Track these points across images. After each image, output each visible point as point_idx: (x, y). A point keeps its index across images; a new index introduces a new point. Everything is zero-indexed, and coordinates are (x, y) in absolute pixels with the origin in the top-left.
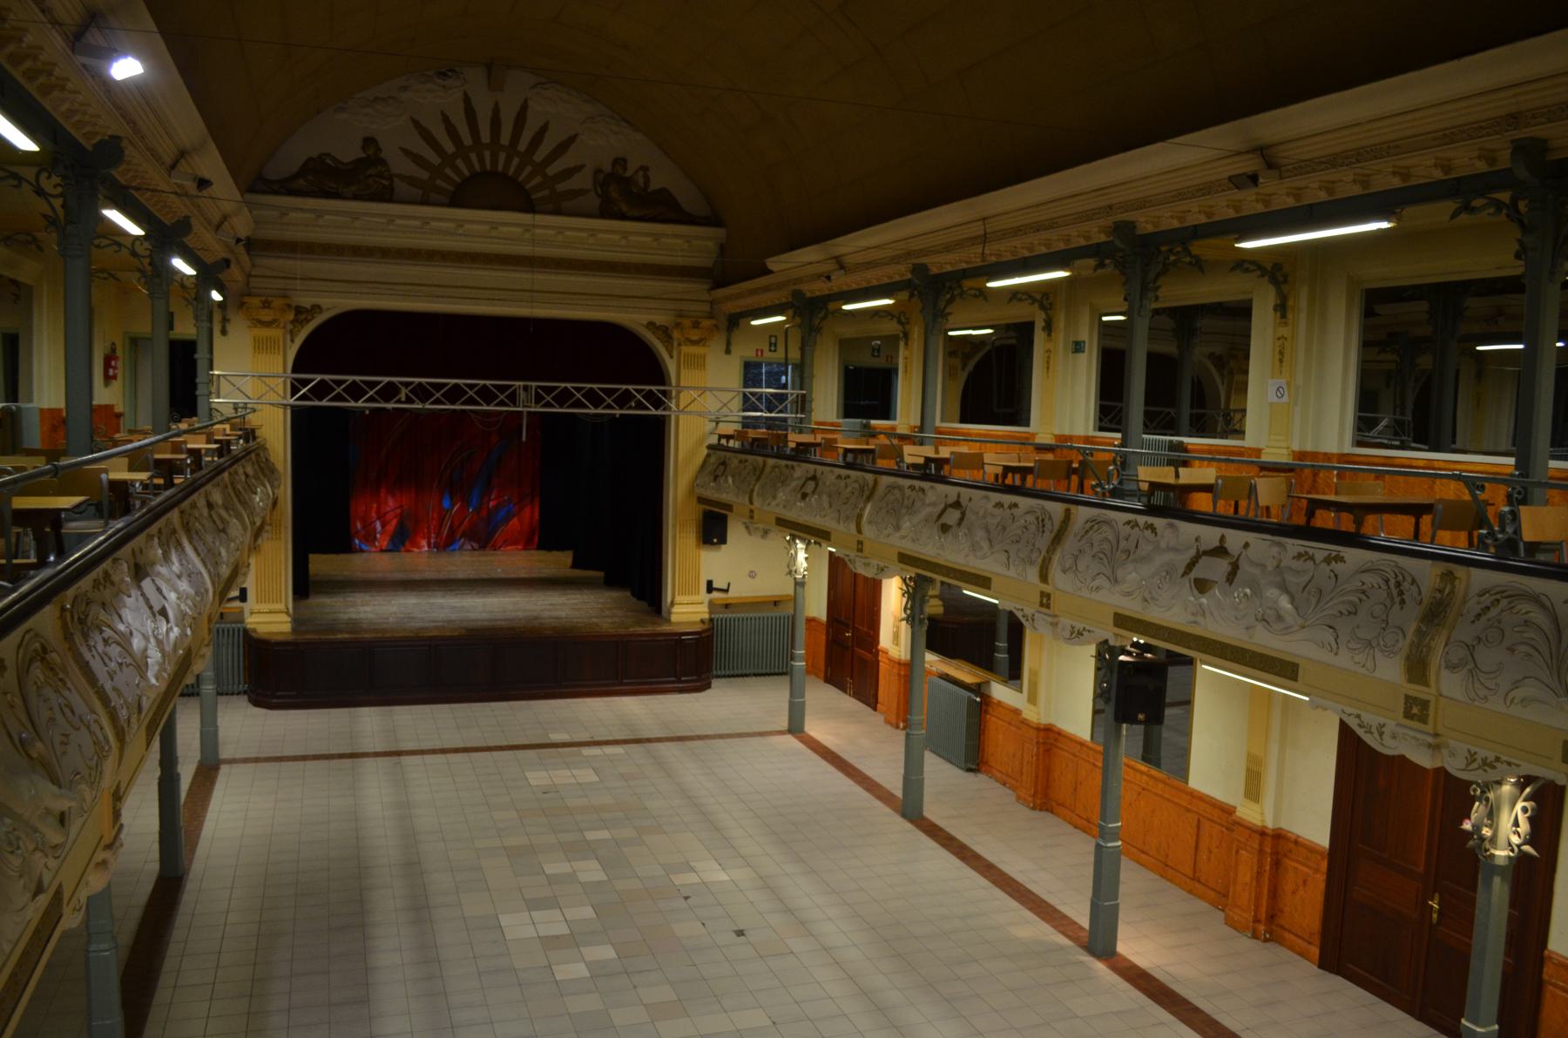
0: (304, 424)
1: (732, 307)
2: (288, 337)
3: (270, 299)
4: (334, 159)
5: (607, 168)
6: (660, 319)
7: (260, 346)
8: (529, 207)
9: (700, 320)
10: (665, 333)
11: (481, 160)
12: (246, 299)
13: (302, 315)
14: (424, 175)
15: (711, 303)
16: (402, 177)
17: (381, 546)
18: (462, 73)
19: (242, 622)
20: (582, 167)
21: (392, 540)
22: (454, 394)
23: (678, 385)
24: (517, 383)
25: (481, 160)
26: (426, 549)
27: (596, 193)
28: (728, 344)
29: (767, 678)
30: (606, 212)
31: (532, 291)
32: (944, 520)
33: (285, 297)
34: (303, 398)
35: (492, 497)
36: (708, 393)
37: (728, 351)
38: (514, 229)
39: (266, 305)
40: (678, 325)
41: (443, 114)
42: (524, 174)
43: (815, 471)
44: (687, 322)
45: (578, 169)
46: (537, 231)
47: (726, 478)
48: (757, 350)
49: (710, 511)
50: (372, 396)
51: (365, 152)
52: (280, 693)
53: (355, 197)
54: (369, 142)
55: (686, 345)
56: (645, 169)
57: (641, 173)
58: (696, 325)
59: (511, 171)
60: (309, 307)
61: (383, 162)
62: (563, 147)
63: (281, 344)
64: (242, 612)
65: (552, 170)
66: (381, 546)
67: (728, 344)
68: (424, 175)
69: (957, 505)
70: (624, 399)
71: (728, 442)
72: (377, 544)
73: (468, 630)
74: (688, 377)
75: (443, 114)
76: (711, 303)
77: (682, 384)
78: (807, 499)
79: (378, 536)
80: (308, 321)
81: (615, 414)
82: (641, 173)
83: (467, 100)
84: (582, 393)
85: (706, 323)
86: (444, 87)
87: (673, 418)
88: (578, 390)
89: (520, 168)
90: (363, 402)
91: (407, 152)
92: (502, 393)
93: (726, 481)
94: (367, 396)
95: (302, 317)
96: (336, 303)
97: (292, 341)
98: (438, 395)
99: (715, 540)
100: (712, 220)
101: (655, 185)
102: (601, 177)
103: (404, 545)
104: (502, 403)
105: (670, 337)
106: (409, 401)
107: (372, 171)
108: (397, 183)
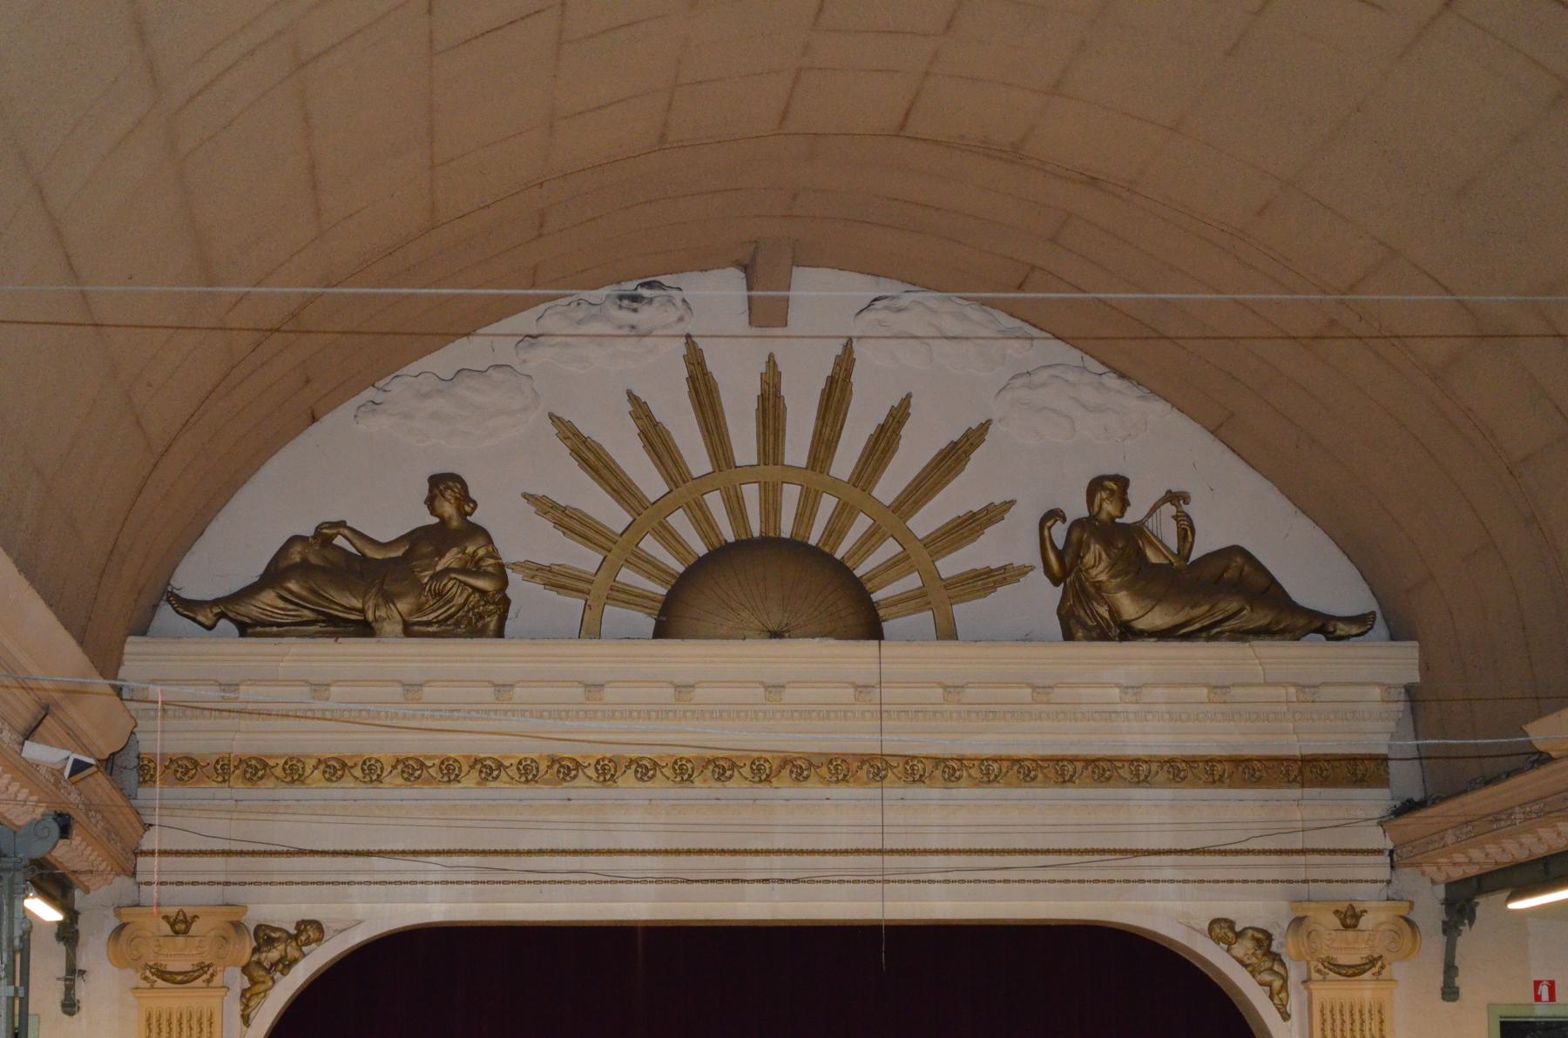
5: (1077, 508)
6: (1251, 909)
8: (872, 629)
11: (736, 507)
25: (736, 507)
37: (1450, 992)
41: (632, 397)
48: (1537, 984)
51: (433, 512)
54: (444, 485)
57: (1169, 509)
62: (952, 458)
68: (585, 559)
91: (545, 506)
102: (1059, 533)
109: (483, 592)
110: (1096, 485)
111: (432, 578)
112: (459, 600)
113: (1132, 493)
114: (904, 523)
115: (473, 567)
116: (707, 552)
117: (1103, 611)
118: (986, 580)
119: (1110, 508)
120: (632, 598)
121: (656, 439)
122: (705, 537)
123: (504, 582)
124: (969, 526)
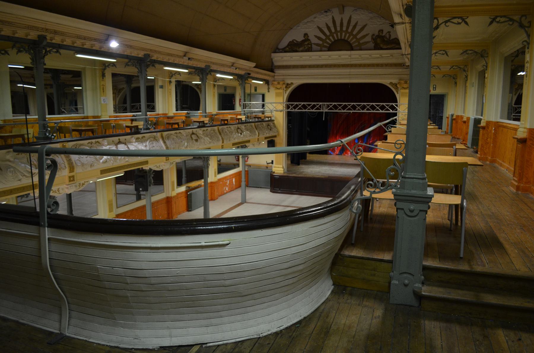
0: (290, 116)
2: (285, 92)
3: (279, 82)
4: (296, 41)
5: (377, 33)
6: (395, 81)
7: (277, 95)
8: (352, 49)
10: (395, 85)
11: (337, 36)
12: (273, 82)
13: (288, 86)
14: (321, 42)
16: (315, 44)
17: (336, 153)
18: (331, 10)
19: (272, 169)
20: (369, 34)
21: (340, 151)
24: (321, 103)
25: (337, 36)
26: (350, 155)
27: (372, 42)
29: (253, 188)
30: (377, 47)
33: (283, 81)
35: (371, 139)
36: (402, 105)
38: (316, 57)
39: (279, 83)
41: (326, 24)
42: (350, 39)
43: (238, 126)
44: (403, 82)
49: (326, 142)
50: (300, 107)
51: (304, 38)
52: (281, 189)
53: (302, 51)
54: (306, 35)
56: (389, 32)
57: (388, 34)
60: (290, 83)
61: (309, 40)
63: (282, 94)
64: (272, 166)
65: (358, 37)
66: (336, 153)
68: (321, 42)
70: (373, 108)
71: (268, 119)
72: (335, 152)
73: (329, 177)
75: (326, 24)
79: (336, 150)
80: (290, 87)
81: (350, 112)
82: (388, 34)
83: (333, 18)
84: (377, 109)
86: (326, 15)
88: (387, 105)
89: (333, 37)
90: (297, 110)
91: (316, 36)
94: (298, 107)
95: (288, 86)
96: (297, 82)
97: (286, 93)
98: (349, 107)
102: (374, 37)
103: (343, 153)
105: (397, 86)
106: (292, 109)
107: (306, 43)
108: (313, 46)
110: (379, 31)
111: (119, 161)
112: (306, 48)
113: (384, 32)
114: (337, 31)
116: (406, 136)
118: (367, 43)
119: (381, 34)
120: (325, 47)
121: (329, 28)
122: (334, 39)
123: (312, 45)
124: (364, 36)
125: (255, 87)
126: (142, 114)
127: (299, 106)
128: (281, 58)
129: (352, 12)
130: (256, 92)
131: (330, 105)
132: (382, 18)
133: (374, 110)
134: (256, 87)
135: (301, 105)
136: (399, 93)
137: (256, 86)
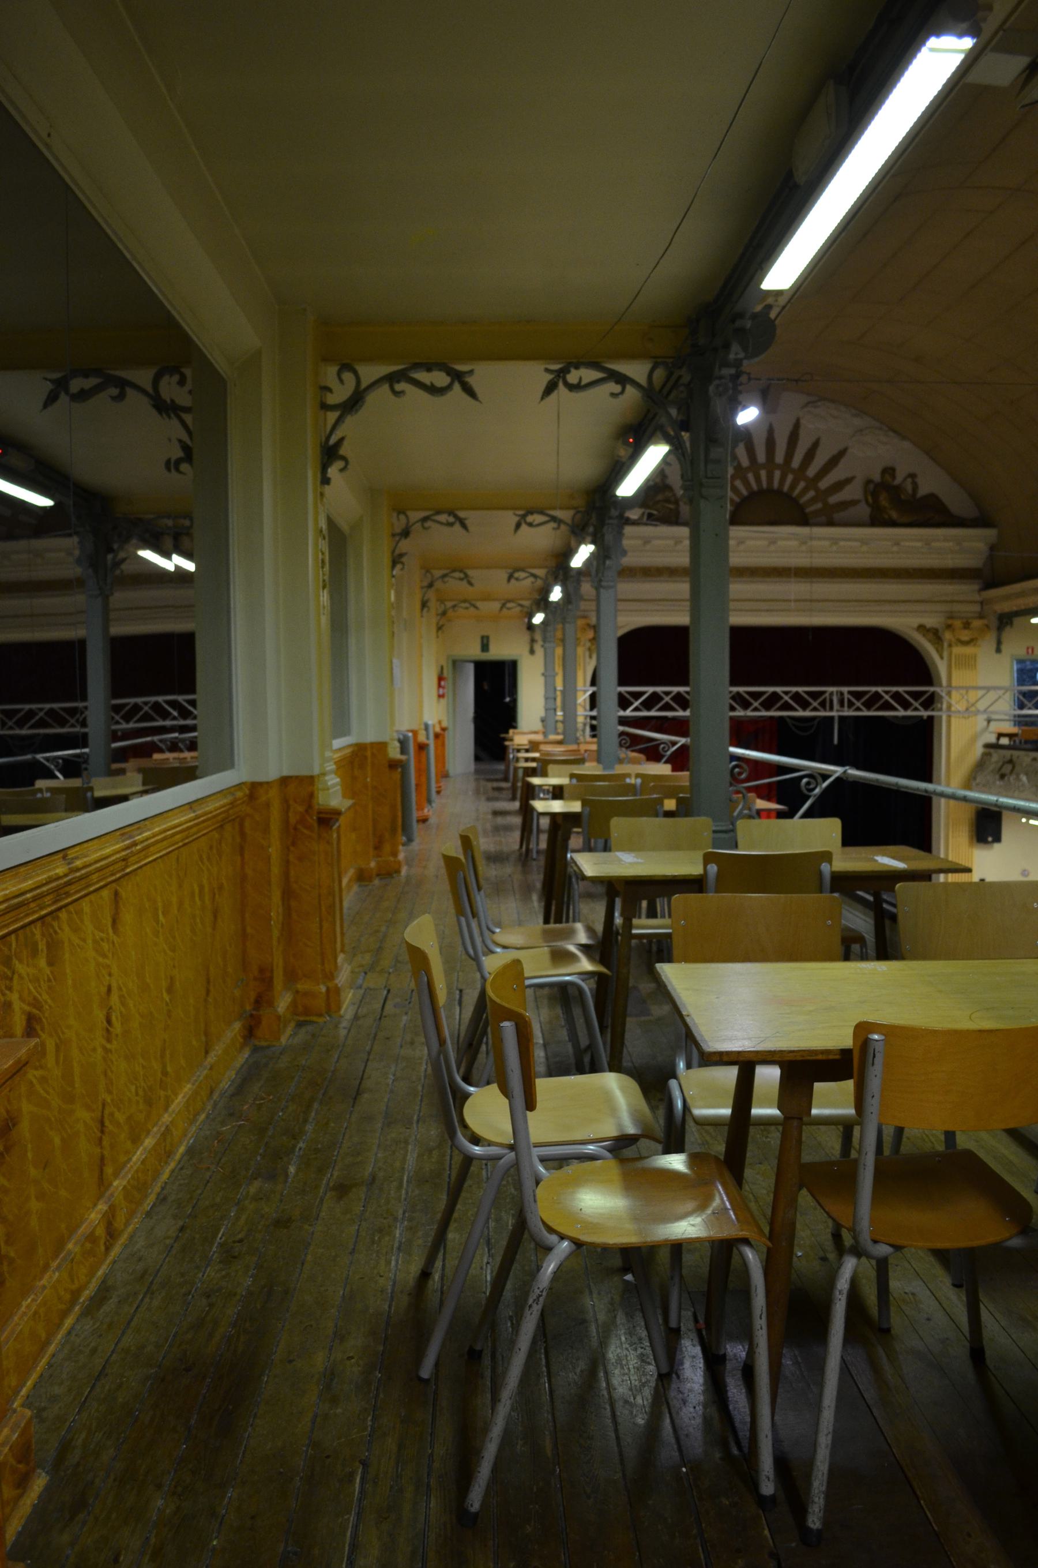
1: (1006, 607)
5: (877, 477)
6: (930, 622)
8: (803, 520)
9: (970, 621)
10: (935, 635)
11: (758, 479)
15: (982, 603)
22: (771, 701)
23: (949, 685)
25: (758, 479)
28: (999, 643)
30: (877, 520)
31: (811, 601)
32: (1003, 771)
34: (636, 709)
37: (998, 650)
40: (949, 627)
43: (1012, 756)
45: (848, 481)
46: (815, 543)
47: (1018, 775)
48: (1028, 648)
55: (957, 645)
57: (909, 480)
58: (967, 626)
59: (786, 488)
62: (833, 462)
67: (999, 643)
69: (1011, 761)
74: (960, 677)
76: (982, 603)
77: (954, 683)
78: (1006, 778)
81: (921, 717)
82: (909, 480)
84: (782, 702)
85: (977, 623)
87: (944, 718)
92: (756, 700)
93: (1018, 779)
99: (990, 839)
100: (981, 521)
101: (922, 491)
102: (871, 486)
104: (815, 709)
109: (671, 509)
115: (667, 501)
117: (886, 517)
118: (844, 505)
121: (810, 455)
124: (839, 486)
125: (483, 638)
126: (91, 751)
127: (641, 704)
128: (640, 542)
129: (803, 407)
130: (485, 654)
131: (632, 700)
132: (891, 434)
133: (808, 710)
134: (488, 638)
135: (640, 701)
136: (945, 654)
137: (486, 634)
